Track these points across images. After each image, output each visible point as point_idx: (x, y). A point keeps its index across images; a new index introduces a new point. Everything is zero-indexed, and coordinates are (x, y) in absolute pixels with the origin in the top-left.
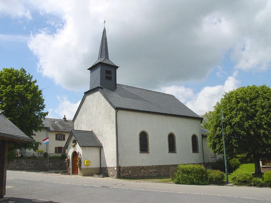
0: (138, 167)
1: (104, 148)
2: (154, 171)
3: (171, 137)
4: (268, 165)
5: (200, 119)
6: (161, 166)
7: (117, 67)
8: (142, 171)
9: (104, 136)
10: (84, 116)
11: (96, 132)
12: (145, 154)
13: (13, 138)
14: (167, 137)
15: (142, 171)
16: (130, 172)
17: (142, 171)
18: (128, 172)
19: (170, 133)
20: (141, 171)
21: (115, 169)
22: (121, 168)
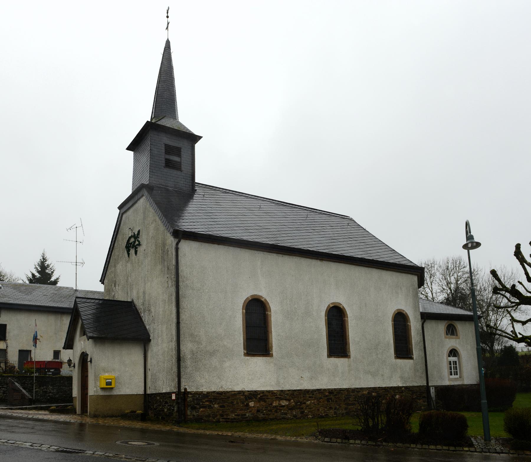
0: (240, 392)
1: (152, 342)
2: (287, 405)
3: (336, 316)
4: (1, 397)
5: (418, 273)
6: (307, 391)
7: (196, 138)
8: (252, 404)
9: (153, 310)
10: (119, 267)
11: (139, 304)
12: (259, 358)
13: (504, 435)
14: (323, 314)
15: (250, 404)
16: (216, 406)
17: (252, 404)
18: (210, 407)
19: (331, 306)
20: (248, 405)
21: (174, 397)
22: (190, 396)
